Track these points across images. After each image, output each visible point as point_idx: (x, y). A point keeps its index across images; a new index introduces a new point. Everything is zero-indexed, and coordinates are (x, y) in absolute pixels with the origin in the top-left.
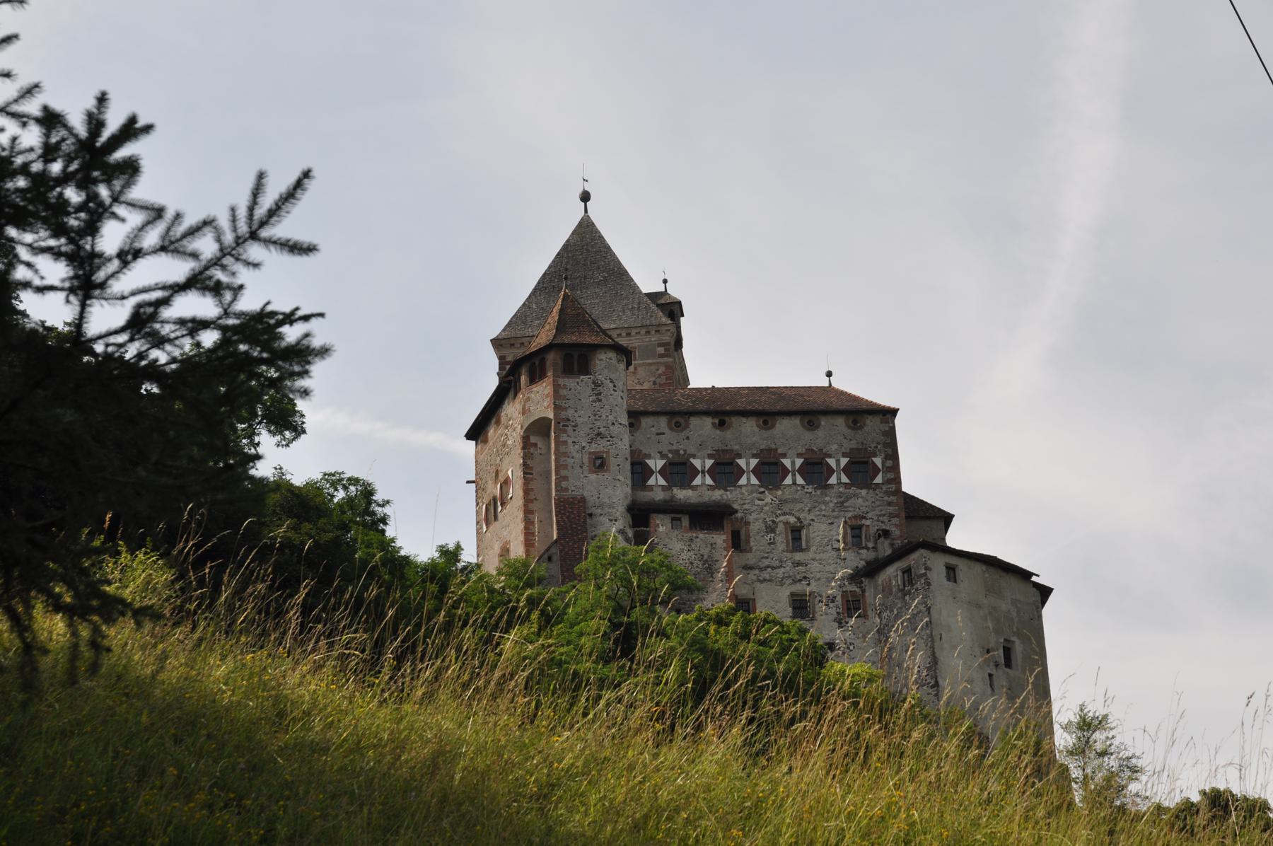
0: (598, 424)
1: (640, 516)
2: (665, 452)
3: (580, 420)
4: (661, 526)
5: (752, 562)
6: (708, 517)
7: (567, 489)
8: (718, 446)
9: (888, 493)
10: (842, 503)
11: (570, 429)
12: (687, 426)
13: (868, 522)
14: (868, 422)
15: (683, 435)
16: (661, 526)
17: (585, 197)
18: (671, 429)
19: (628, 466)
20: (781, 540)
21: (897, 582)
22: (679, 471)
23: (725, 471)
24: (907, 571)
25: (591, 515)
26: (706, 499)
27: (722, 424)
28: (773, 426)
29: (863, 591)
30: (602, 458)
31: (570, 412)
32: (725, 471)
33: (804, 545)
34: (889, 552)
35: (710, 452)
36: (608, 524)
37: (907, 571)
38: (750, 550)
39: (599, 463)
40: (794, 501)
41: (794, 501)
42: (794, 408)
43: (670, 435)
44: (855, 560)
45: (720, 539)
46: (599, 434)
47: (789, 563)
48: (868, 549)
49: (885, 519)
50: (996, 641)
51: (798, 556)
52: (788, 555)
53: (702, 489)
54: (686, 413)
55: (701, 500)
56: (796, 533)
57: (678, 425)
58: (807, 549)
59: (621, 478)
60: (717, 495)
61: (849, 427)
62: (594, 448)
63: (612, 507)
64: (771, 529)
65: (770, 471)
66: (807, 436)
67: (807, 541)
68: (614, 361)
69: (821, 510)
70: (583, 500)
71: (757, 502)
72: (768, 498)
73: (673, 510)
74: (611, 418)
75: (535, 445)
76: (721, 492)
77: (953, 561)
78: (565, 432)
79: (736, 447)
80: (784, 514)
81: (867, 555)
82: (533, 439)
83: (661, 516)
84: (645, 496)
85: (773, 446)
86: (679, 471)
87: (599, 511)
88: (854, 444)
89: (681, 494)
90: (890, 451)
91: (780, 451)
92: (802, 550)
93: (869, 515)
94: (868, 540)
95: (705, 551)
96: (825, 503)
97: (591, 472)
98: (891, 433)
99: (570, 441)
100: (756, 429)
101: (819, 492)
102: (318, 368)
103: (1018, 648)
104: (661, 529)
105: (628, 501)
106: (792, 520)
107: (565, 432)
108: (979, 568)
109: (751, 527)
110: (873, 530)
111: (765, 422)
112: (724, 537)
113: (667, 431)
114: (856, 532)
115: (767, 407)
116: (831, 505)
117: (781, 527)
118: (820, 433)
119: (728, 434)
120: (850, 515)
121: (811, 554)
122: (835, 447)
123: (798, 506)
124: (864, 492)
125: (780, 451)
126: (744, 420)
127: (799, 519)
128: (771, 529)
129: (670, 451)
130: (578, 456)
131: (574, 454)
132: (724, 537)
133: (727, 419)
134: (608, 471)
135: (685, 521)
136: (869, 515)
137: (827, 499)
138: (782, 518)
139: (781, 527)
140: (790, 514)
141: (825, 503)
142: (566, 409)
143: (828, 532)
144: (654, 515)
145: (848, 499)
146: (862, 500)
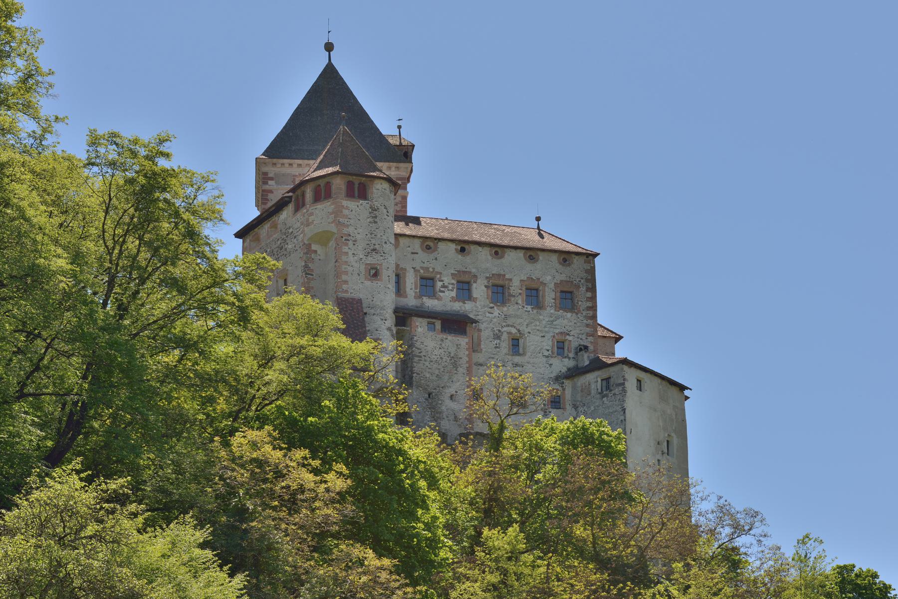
0: (373, 241)
1: (403, 317)
2: (418, 268)
3: (358, 237)
4: (420, 327)
5: (481, 361)
6: (455, 324)
7: (346, 291)
8: (460, 268)
9: (587, 317)
10: (552, 321)
11: (350, 243)
12: (435, 250)
13: (570, 338)
14: (575, 261)
15: (432, 256)
16: (420, 327)
17: (329, 47)
18: (423, 250)
19: (524, 292)
20: (505, 345)
22: (428, 283)
23: (464, 287)
24: (608, 380)
25: (366, 314)
26: (448, 308)
27: (463, 250)
28: (502, 257)
29: (564, 390)
30: (376, 269)
31: (351, 230)
32: (464, 287)
33: (521, 351)
34: (587, 363)
35: (453, 272)
36: (380, 322)
38: (481, 351)
40: (516, 316)
41: (516, 316)
42: (519, 245)
44: (561, 365)
45: (463, 341)
46: (374, 250)
47: (510, 364)
48: (569, 358)
49: (584, 337)
50: (663, 436)
51: (517, 359)
52: (510, 357)
53: (446, 301)
54: (436, 239)
55: (445, 309)
56: (515, 344)
57: (428, 248)
58: (524, 354)
59: (390, 286)
60: (457, 306)
61: (560, 263)
62: (370, 260)
63: (382, 308)
64: (498, 337)
66: (529, 267)
67: (524, 348)
68: (388, 191)
69: (536, 325)
70: (360, 301)
71: (488, 315)
72: (496, 312)
73: (429, 315)
74: (384, 237)
75: (315, 252)
76: (461, 304)
78: (347, 245)
79: (473, 270)
80: (508, 326)
81: (571, 363)
83: (420, 319)
85: (502, 272)
86: (428, 283)
87: (372, 311)
88: (563, 277)
89: (430, 304)
90: (590, 285)
91: (507, 276)
92: (520, 355)
93: (572, 333)
94: (569, 351)
95: (453, 350)
96: (539, 320)
97: (366, 279)
98: (592, 272)
99: (350, 253)
100: (490, 258)
101: (535, 311)
103: (675, 441)
104: (419, 330)
105: (393, 307)
106: (514, 331)
107: (347, 245)
109: (482, 333)
110: (574, 344)
111: (496, 253)
112: (466, 340)
113: (420, 251)
114: (560, 347)
115: (498, 242)
116: (544, 322)
117: (505, 336)
118: (538, 266)
119: (468, 259)
120: (557, 331)
121: (525, 359)
122: (549, 278)
123: (519, 321)
124: (569, 315)
125: (507, 276)
126: (480, 249)
127: (519, 331)
128: (498, 337)
129: (421, 268)
130: (356, 265)
131: (354, 264)
132: (466, 340)
133: (466, 247)
134: (381, 280)
136: (572, 333)
137: (541, 317)
138: (505, 329)
139: (505, 336)
140: (512, 326)
141: (539, 320)
142: (348, 226)
143: (538, 343)
144: (415, 318)
145: (557, 318)
146: (567, 321)
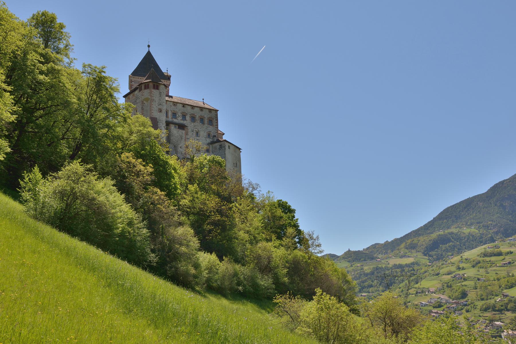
6: (182, 127)
17: (149, 46)
20: (195, 134)
21: (218, 147)
24: (221, 145)
31: (154, 98)
32: (184, 116)
37: (221, 145)
39: (160, 111)
43: (173, 107)
45: (184, 132)
51: (198, 138)
60: (182, 122)
62: (159, 107)
65: (193, 119)
66: (201, 112)
72: (192, 124)
73: (175, 124)
77: (230, 145)
82: (144, 102)
84: (168, 119)
89: (175, 120)
95: (181, 134)
98: (217, 115)
102: (299, 220)
108: (233, 147)
110: (213, 135)
114: (209, 135)
119: (185, 109)
128: (193, 131)
135: (177, 126)
146: (211, 128)
